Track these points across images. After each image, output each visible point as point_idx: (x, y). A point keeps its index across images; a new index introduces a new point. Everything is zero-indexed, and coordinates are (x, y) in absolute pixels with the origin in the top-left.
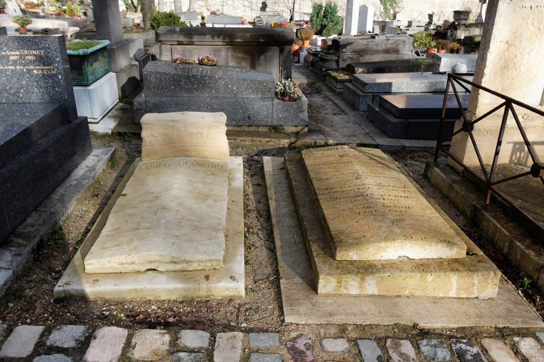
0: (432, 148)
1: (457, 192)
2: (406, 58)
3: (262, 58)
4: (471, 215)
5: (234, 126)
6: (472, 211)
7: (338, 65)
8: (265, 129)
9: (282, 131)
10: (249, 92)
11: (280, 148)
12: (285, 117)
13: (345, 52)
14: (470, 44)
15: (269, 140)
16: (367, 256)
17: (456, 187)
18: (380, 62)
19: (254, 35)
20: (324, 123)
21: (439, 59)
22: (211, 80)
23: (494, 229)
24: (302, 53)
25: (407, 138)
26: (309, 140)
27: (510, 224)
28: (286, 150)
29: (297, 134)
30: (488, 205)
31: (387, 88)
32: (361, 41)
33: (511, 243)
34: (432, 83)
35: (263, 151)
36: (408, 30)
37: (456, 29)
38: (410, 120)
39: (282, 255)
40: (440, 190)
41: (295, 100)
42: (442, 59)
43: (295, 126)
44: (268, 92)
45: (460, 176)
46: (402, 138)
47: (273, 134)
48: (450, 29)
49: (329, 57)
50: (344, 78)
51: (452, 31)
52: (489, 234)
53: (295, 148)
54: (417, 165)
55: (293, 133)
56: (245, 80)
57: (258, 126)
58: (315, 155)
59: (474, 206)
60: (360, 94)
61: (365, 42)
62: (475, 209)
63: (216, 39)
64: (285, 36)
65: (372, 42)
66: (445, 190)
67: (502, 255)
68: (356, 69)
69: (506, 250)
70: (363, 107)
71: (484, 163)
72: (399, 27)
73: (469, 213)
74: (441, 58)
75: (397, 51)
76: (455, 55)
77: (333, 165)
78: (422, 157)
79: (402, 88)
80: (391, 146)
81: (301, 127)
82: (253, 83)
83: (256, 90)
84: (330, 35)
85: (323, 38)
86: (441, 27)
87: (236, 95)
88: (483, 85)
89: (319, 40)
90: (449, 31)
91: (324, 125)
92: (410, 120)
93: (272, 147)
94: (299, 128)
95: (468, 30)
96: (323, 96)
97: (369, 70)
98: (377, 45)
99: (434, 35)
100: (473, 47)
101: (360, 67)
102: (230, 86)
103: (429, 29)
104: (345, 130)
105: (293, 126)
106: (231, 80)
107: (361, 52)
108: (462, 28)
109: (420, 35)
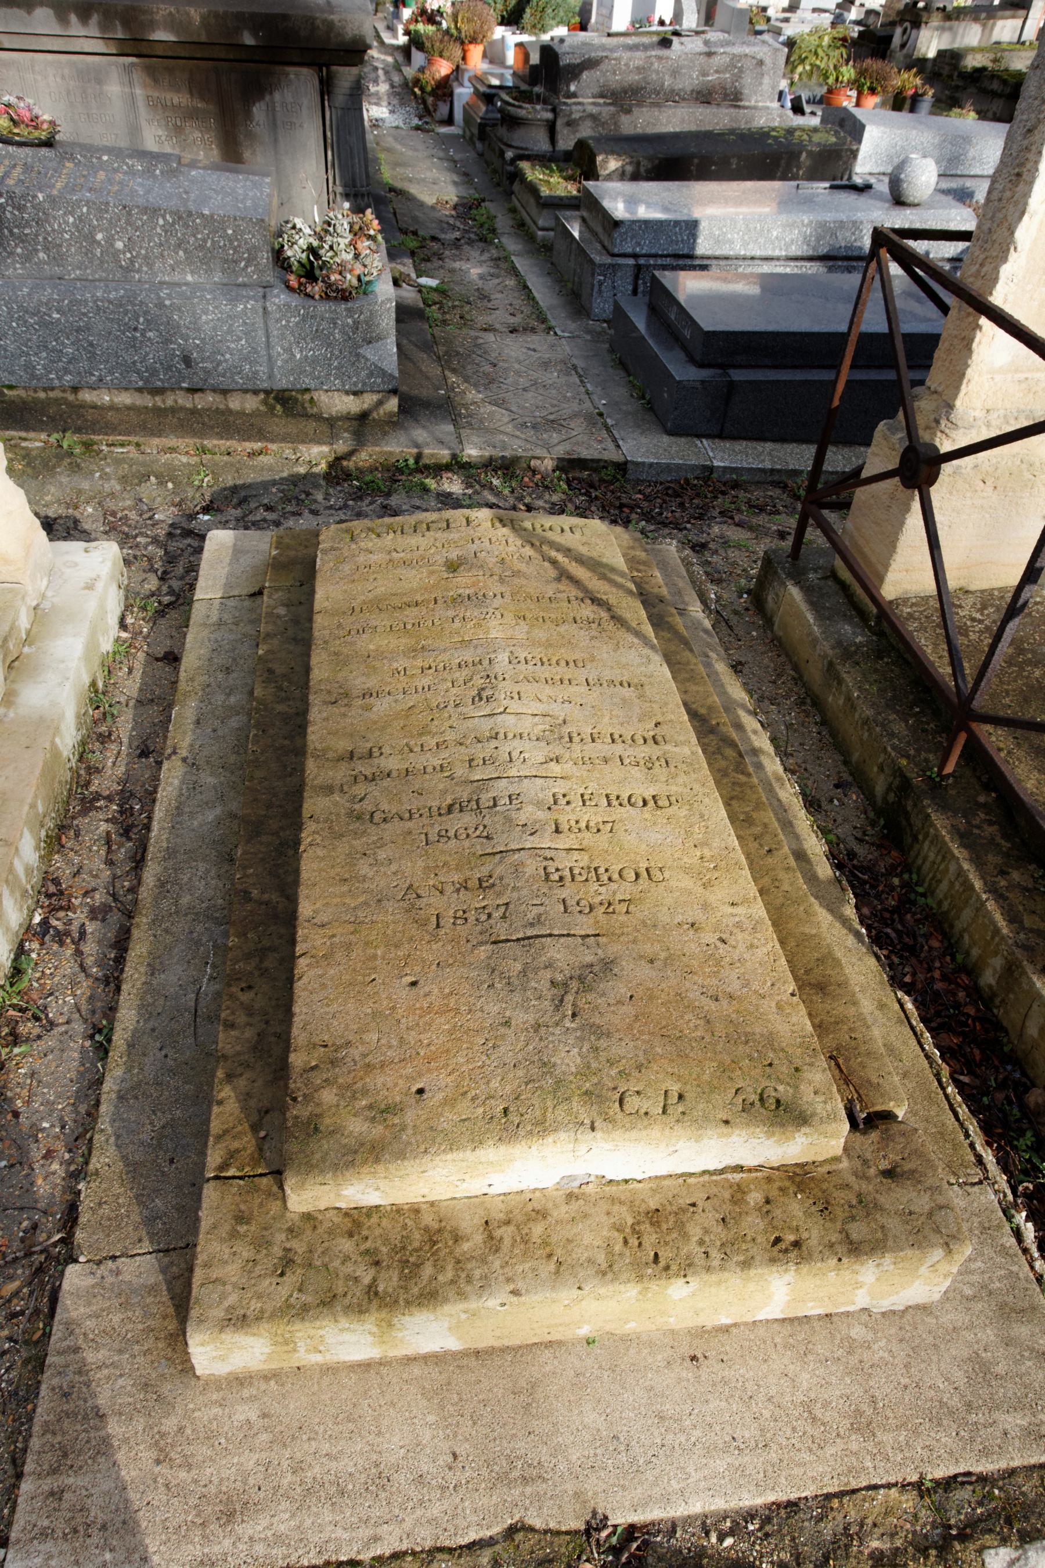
0: (796, 473)
1: (849, 699)
2: (761, 122)
3: (259, 111)
4: (885, 799)
5: (139, 390)
6: (889, 788)
7: (553, 140)
8: (251, 403)
9: (310, 411)
10: (178, 263)
11: (295, 480)
12: (315, 361)
13: (574, 95)
14: (950, 77)
15: (258, 445)
16: (426, 1191)
17: (850, 676)
18: (676, 136)
19: (216, 15)
20: (470, 369)
21: (857, 130)
22: (21, 208)
23: (957, 886)
24: (458, 91)
25: (721, 435)
26: (396, 447)
27: (1016, 875)
28: (317, 486)
29: (361, 423)
30: (948, 776)
31: (678, 246)
32: (626, 55)
33: (1011, 971)
34: (822, 225)
35: (235, 489)
36: (786, 20)
37: (917, 24)
38: (738, 375)
39: (121, 1098)
40: (796, 668)
41: (344, 296)
42: (868, 129)
43: (355, 393)
44: (249, 261)
45: (870, 628)
46: (708, 436)
47: (279, 424)
48: (902, 21)
49: (526, 111)
50: (561, 192)
51: (905, 31)
52: (940, 893)
53: (348, 476)
54: (738, 547)
55: (348, 417)
56: (154, 212)
57: (225, 392)
58: (361, 559)
59: (899, 772)
60: (597, 259)
61: (638, 58)
62: (905, 786)
63: (75, 27)
64: (330, 25)
65: (660, 58)
66: (815, 674)
67: (976, 992)
68: (599, 158)
69: (989, 978)
70: (601, 306)
71: (953, 582)
72: (764, 9)
73: (880, 789)
74: (863, 127)
75: (733, 97)
76: (904, 116)
77: (411, 613)
78: (762, 509)
79: (731, 242)
80: (668, 465)
81: (375, 397)
82: (186, 226)
83: (203, 256)
84: (543, 30)
85: (525, 38)
86: (877, 13)
87: (128, 269)
88: (999, 298)
89: (509, 38)
90: (899, 31)
91: (466, 380)
92: (738, 375)
93: (267, 477)
94: (369, 400)
95: (950, 29)
96: (494, 253)
97: (638, 164)
98: (675, 73)
99: (855, 43)
100: (957, 87)
101: (612, 152)
102: (99, 237)
103: (844, 22)
104: (531, 398)
105: (347, 393)
106: (102, 209)
107: (625, 98)
108: (936, 20)
109: (814, 41)
